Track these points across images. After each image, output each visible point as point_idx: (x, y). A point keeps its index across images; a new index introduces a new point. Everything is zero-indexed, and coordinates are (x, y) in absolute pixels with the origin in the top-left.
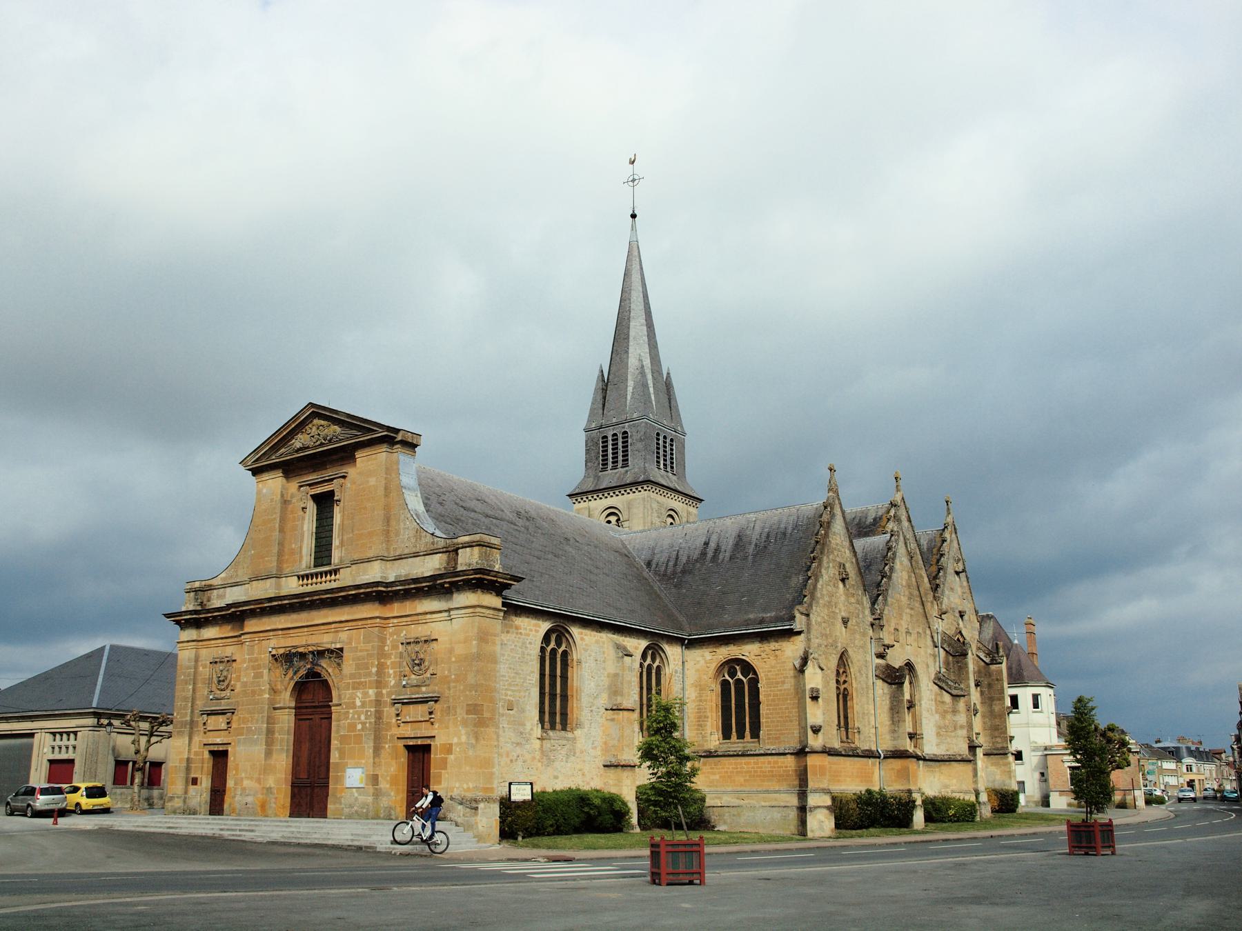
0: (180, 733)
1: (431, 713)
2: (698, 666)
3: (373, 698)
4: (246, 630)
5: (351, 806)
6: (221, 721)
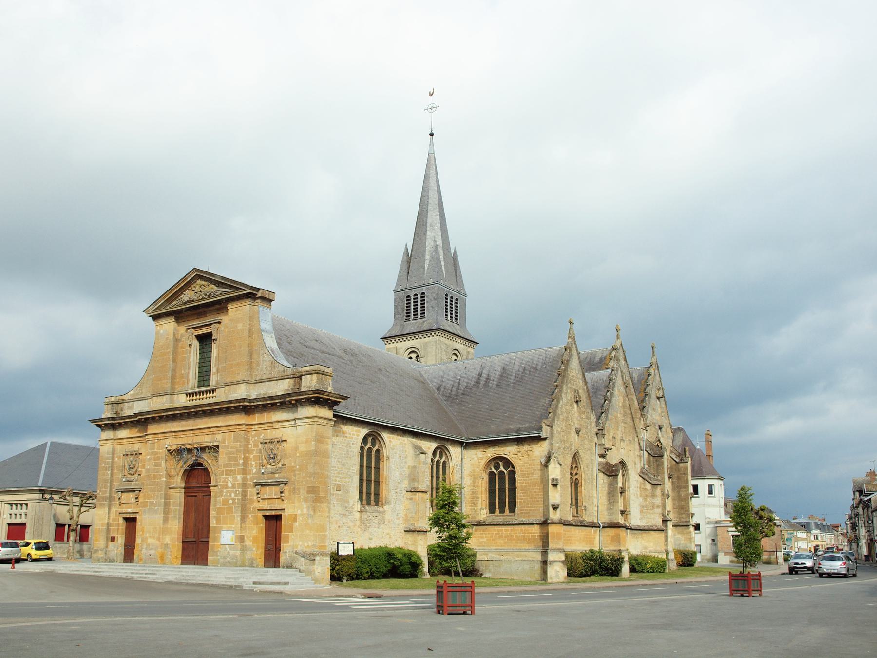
0: (102, 505)
1: (282, 493)
2: (472, 462)
3: (240, 481)
4: (149, 432)
5: (225, 558)
6: (131, 497)
